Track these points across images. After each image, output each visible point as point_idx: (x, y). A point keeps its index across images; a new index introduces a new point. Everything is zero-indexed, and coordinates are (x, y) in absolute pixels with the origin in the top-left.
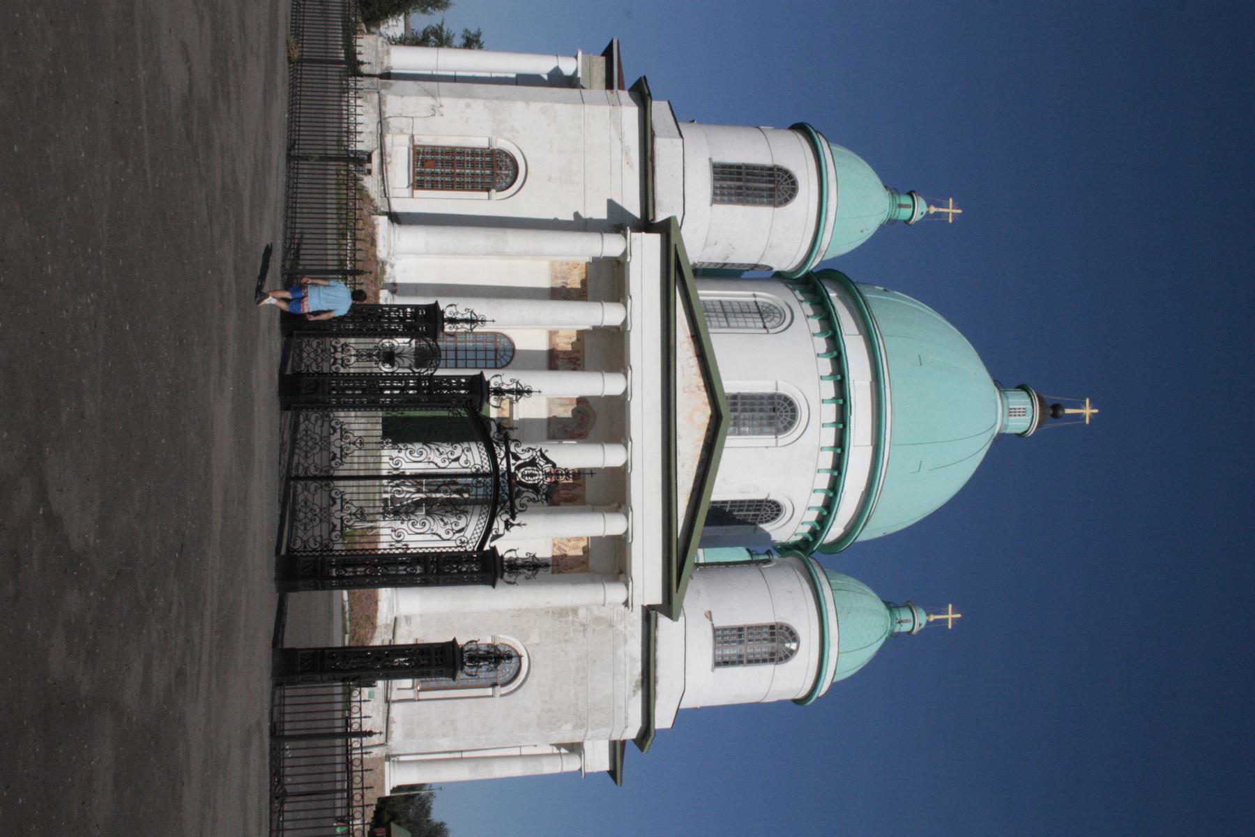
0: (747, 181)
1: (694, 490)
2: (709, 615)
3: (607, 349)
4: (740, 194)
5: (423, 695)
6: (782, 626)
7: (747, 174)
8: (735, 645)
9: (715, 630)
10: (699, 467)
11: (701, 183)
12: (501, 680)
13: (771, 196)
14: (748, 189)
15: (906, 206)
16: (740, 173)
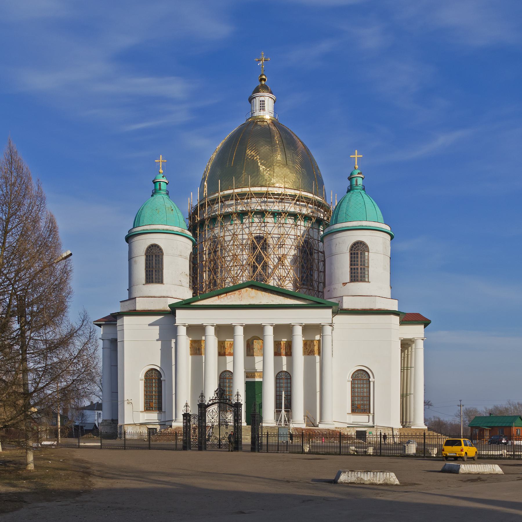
0: (153, 267)
1: (283, 296)
2: (344, 284)
3: (225, 331)
4: (159, 271)
5: (372, 412)
6: (351, 250)
7: (150, 267)
8: (358, 273)
9: (352, 281)
10: (273, 294)
11: (154, 289)
12: (367, 378)
13: (159, 256)
14: (156, 267)
15: (160, 185)
16: (150, 271)
